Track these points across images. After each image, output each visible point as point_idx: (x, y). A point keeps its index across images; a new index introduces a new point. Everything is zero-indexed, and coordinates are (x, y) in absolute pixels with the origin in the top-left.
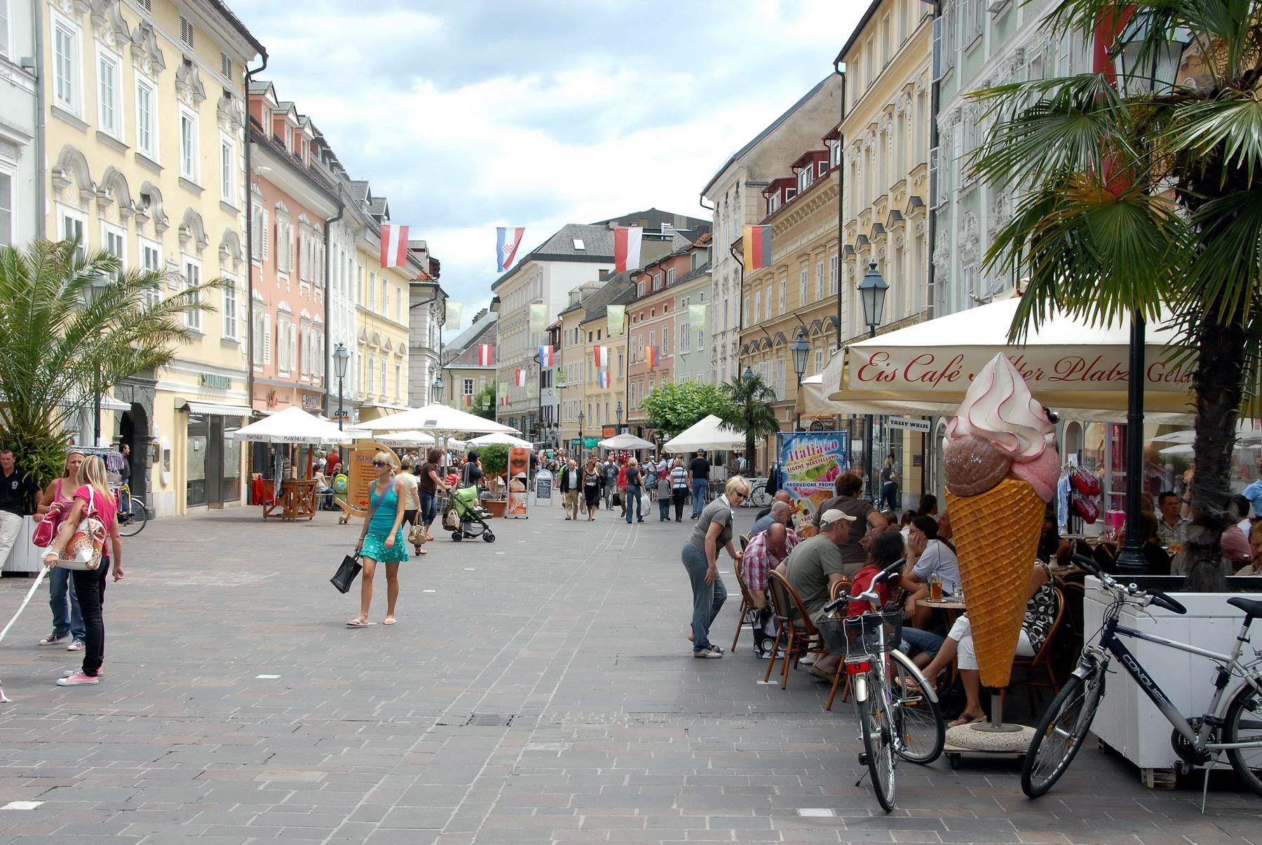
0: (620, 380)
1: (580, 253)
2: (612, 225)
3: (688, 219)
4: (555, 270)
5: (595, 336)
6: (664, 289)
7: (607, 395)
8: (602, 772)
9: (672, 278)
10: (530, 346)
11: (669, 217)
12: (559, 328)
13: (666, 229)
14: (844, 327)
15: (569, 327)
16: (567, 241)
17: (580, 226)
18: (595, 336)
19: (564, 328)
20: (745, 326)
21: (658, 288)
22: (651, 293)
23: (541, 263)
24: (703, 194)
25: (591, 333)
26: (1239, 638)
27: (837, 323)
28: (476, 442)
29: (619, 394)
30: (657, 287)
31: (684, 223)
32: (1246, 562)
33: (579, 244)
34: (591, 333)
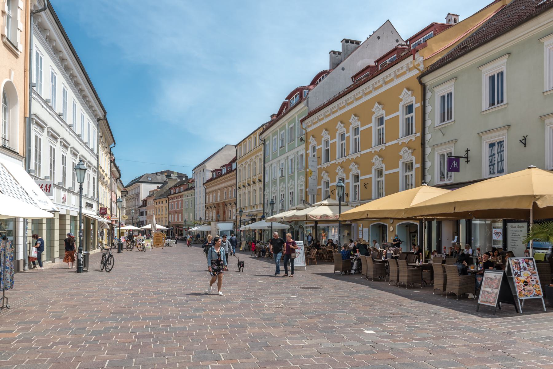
0: (166, 214)
1: (150, 181)
2: (158, 174)
3: (177, 173)
4: (143, 186)
5: (158, 203)
6: (180, 192)
7: (162, 218)
8: (157, 342)
9: (182, 190)
10: (58, 179)
11: (173, 172)
12: (146, 201)
13: (172, 175)
14: (237, 205)
15: (151, 202)
16: (146, 178)
17: (149, 174)
18: (158, 203)
19: (148, 201)
20: (207, 203)
21: (178, 192)
22: (175, 193)
23: (139, 184)
24: (192, 171)
25: (156, 203)
26: (520, 141)
27: (236, 204)
28: (250, 256)
29: (166, 218)
30: (177, 191)
31: (176, 174)
32: (167, 359)
33: (150, 179)
34: (156, 203)
